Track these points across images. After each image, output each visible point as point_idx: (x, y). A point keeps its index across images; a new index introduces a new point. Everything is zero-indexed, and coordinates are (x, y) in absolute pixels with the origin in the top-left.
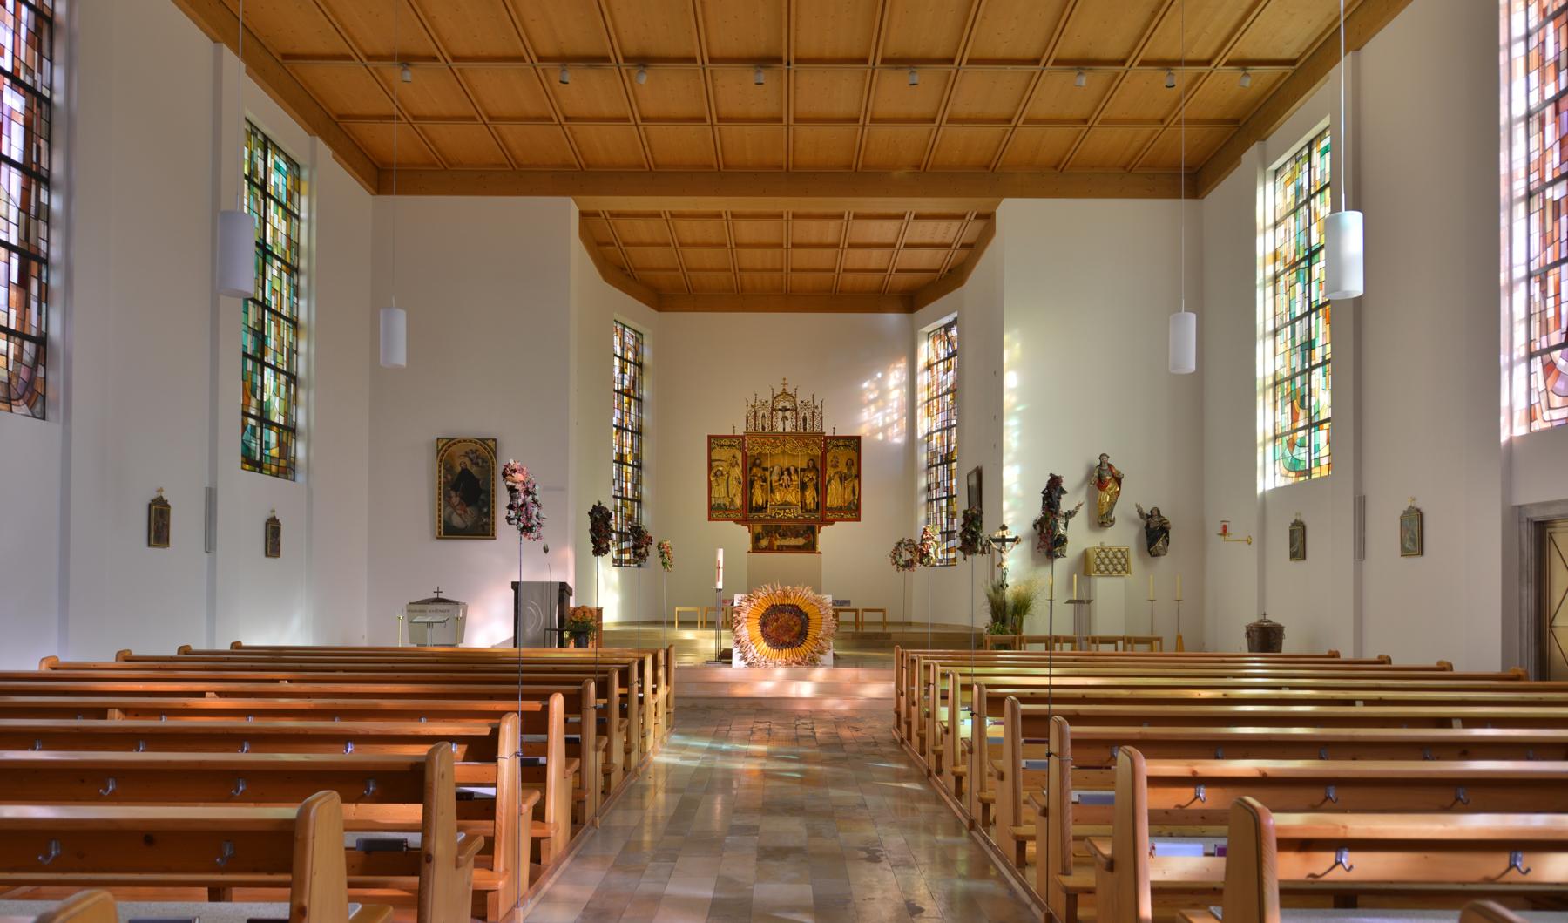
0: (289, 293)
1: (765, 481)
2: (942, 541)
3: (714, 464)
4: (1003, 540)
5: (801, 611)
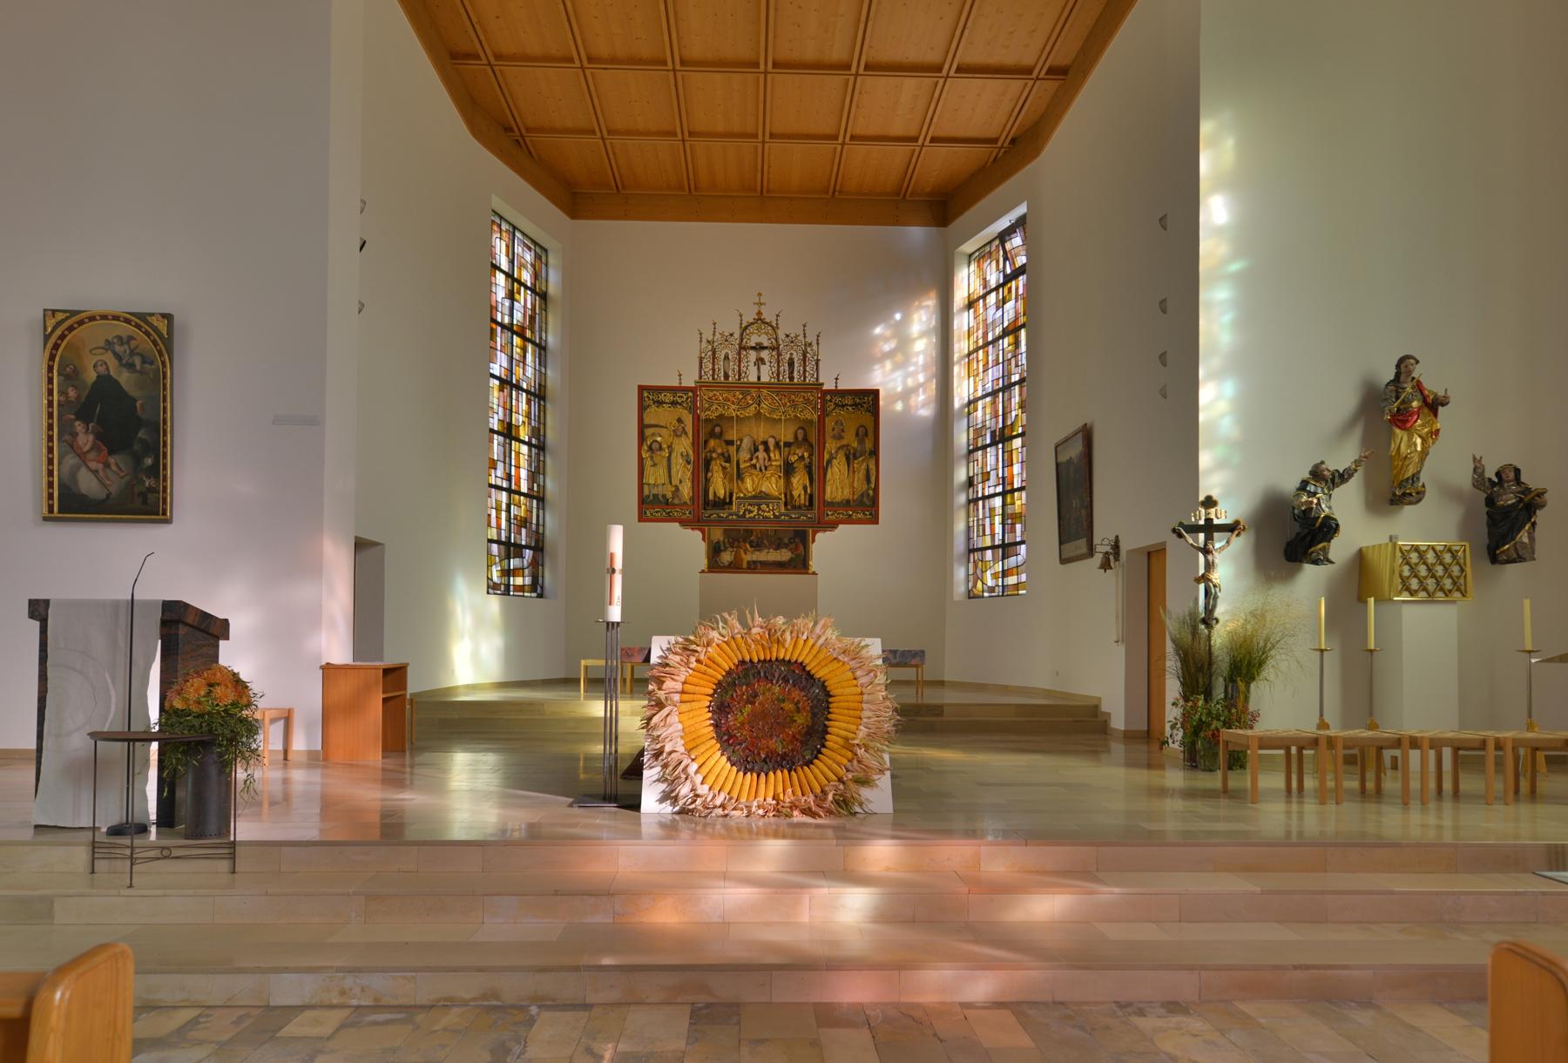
1: (728, 460)
2: (994, 560)
3: (648, 432)
4: (1210, 528)
5: (810, 676)
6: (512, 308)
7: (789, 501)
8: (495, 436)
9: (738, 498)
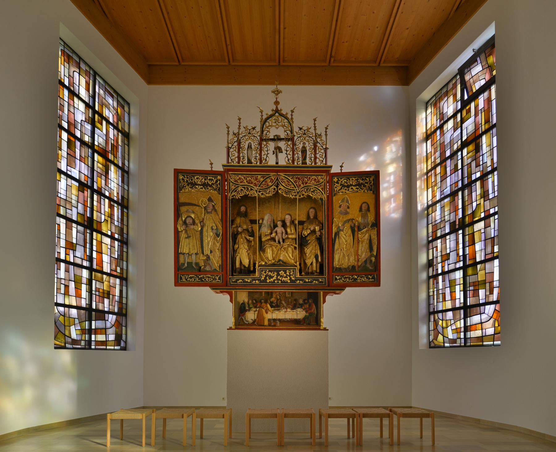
1: (252, 234)
7: (303, 269)
8: (74, 225)
9: (261, 265)
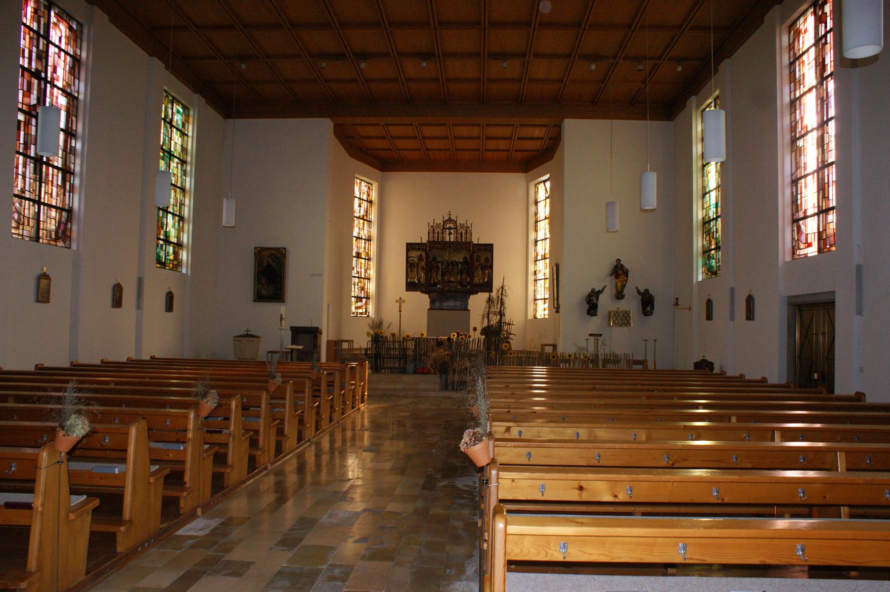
0: (181, 175)
3: (409, 259)
6: (360, 210)
